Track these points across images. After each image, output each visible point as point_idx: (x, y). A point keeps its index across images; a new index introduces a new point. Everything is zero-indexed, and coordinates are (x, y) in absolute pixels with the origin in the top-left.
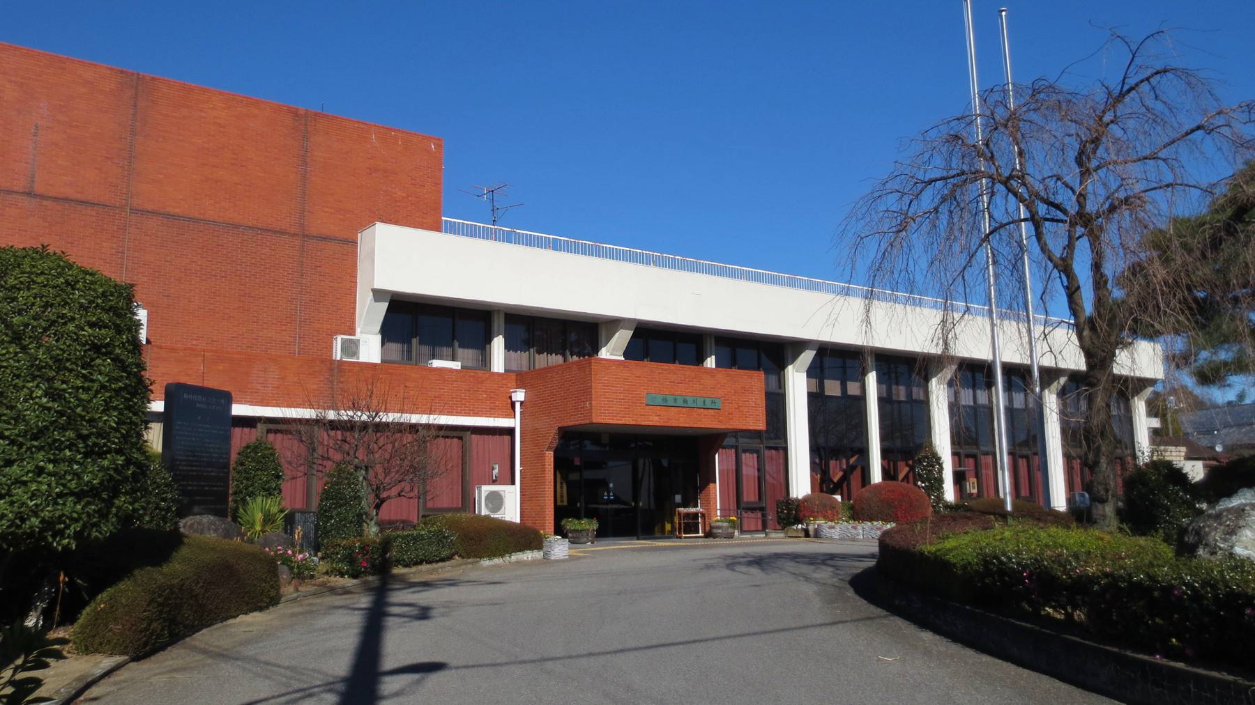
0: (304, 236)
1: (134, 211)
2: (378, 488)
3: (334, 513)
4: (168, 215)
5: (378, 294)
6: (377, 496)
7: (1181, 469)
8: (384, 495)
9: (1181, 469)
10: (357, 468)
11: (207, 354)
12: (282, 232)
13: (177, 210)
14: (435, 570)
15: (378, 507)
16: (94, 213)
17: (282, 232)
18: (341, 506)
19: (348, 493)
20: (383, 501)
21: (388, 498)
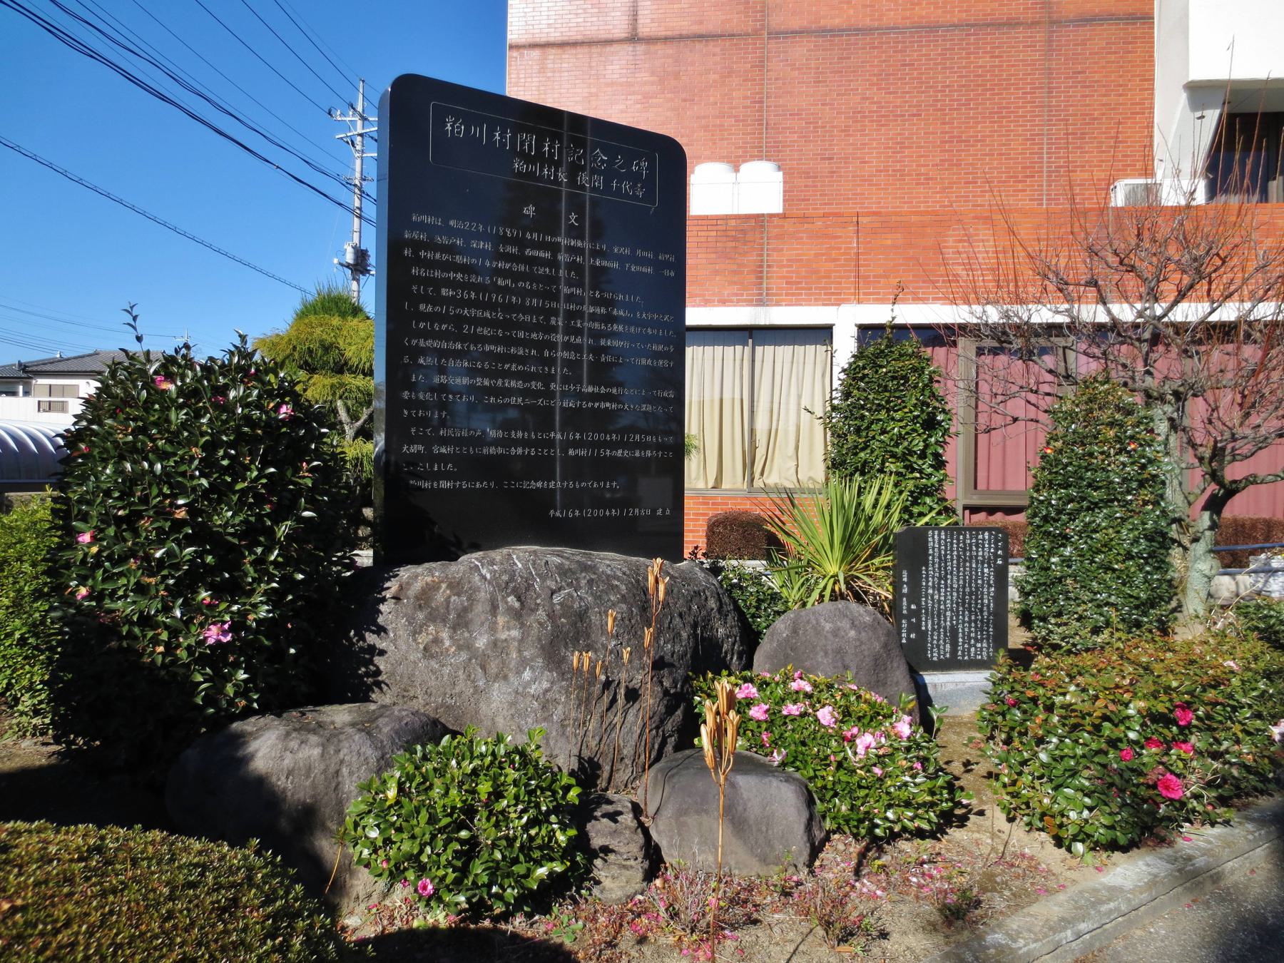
0: (1052, 23)
1: (775, 35)
2: (1218, 453)
3: (1077, 525)
4: (823, 32)
5: (1199, 93)
6: (1215, 476)
7: (561, 945)
8: (1233, 472)
9: (561, 945)
10: (1150, 398)
11: (863, 220)
12: (1012, 24)
13: (837, 21)
14: (786, 432)
15: (1215, 505)
16: (718, 50)
17: (1012, 24)
18: (1094, 506)
19: (1118, 467)
20: (1231, 491)
21: (1251, 480)
